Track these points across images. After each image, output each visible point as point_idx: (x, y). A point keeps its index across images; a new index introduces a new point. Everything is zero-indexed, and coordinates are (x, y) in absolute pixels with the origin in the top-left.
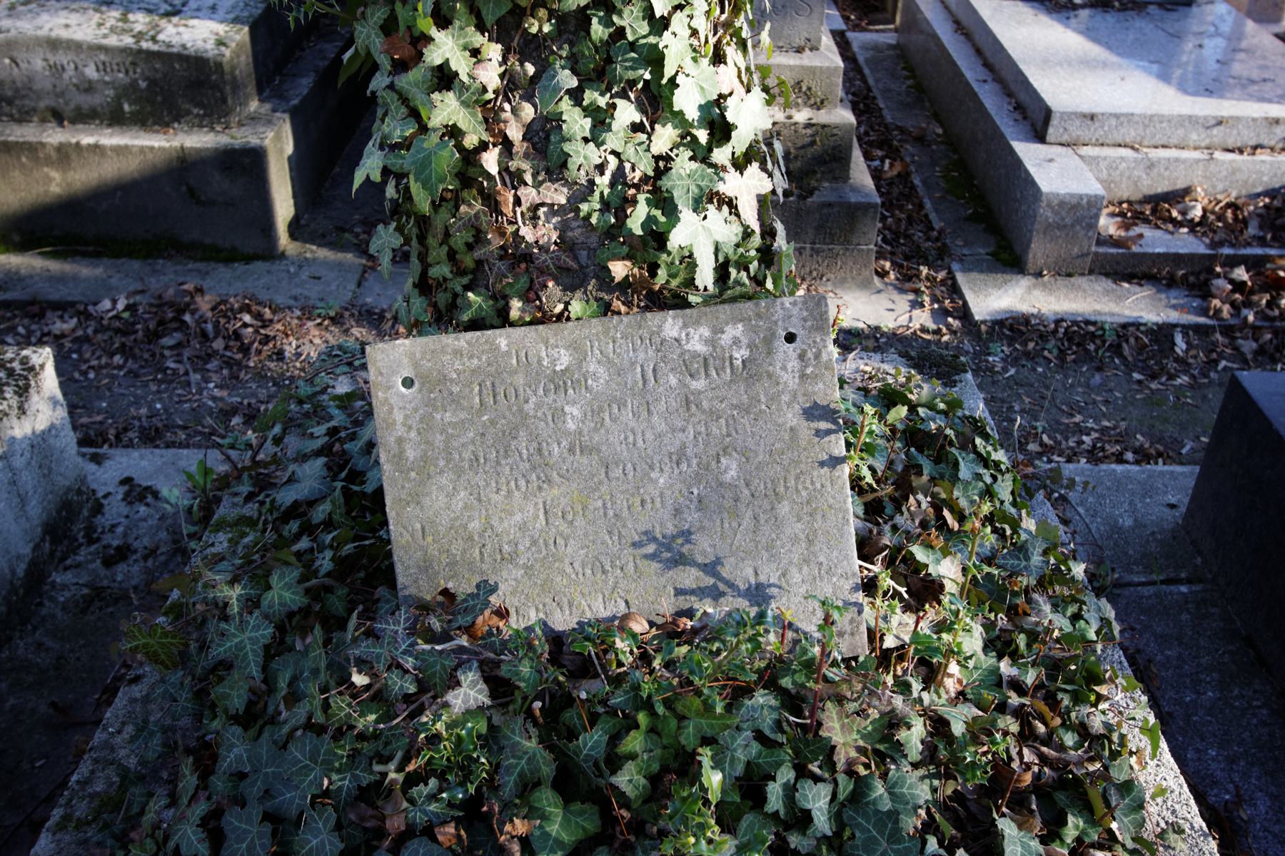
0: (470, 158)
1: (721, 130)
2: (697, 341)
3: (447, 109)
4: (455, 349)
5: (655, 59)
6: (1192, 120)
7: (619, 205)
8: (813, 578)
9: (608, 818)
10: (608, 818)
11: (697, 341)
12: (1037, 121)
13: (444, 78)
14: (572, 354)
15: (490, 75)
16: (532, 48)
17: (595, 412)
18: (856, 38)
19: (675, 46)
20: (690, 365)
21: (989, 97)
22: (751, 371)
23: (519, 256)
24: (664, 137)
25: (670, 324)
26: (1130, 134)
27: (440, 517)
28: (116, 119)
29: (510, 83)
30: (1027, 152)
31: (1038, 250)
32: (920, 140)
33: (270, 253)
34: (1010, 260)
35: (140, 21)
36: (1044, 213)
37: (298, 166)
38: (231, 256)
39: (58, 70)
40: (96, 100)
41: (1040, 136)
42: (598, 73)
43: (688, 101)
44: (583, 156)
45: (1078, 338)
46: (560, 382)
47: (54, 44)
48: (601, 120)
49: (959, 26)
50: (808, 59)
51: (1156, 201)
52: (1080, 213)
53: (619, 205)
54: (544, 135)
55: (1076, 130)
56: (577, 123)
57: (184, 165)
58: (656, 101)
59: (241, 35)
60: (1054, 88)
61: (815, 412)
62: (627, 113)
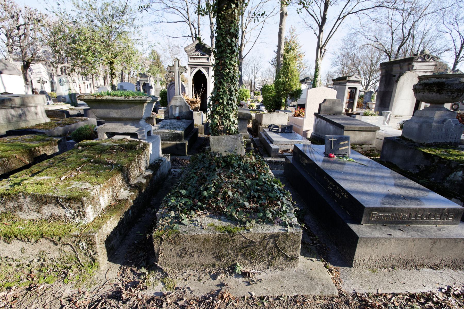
0: (217, 124)
1: (234, 123)
2: (233, 137)
3: (216, 120)
4: (216, 137)
5: (230, 117)
6: (289, 141)
7: (227, 127)
8: (242, 151)
9: (227, 164)
10: (227, 164)
11: (233, 137)
12: (272, 142)
13: (216, 118)
14: (223, 137)
15: (219, 118)
16: (222, 117)
17: (226, 141)
18: (254, 139)
19: (231, 116)
20: (232, 138)
21: (268, 141)
22: (237, 139)
23: (221, 131)
24: (230, 123)
25: (231, 136)
26: (282, 143)
27: (214, 148)
28: (169, 140)
29: (220, 119)
30: (271, 145)
31: (272, 154)
32: (261, 147)
33: (185, 155)
34: (270, 156)
35: (172, 131)
36: (272, 150)
37: (188, 146)
38: (181, 155)
39: (163, 135)
40: (167, 138)
41: (273, 144)
42: (226, 118)
43: (232, 120)
44: (225, 124)
45: (276, 162)
46: (223, 139)
47: (164, 132)
48: (226, 121)
49: (265, 135)
50: (246, 134)
51: (286, 150)
52: (277, 150)
53: (227, 127)
54: (222, 123)
55: (276, 143)
56: (224, 121)
57: (177, 144)
58: (230, 120)
59: (183, 132)
60: (274, 139)
61: (241, 142)
62: (228, 121)
